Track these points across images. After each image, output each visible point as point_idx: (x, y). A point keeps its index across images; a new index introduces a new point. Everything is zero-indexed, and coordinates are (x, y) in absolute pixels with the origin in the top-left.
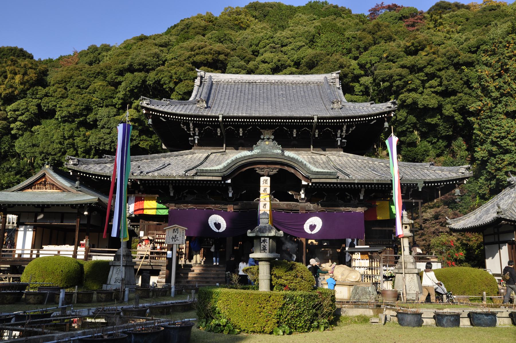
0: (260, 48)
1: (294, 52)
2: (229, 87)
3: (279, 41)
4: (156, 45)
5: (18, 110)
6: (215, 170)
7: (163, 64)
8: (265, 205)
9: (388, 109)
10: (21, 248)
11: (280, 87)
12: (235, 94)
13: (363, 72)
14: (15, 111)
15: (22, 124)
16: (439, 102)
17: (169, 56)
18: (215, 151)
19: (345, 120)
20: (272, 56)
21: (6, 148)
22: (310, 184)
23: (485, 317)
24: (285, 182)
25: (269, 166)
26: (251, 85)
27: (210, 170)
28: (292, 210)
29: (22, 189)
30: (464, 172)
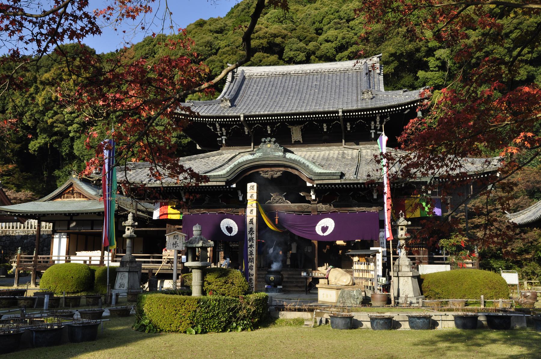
0: (324, 25)
1: (362, 26)
2: (261, 80)
3: (345, 15)
4: (211, 31)
5: (74, 113)
6: (219, 175)
7: (216, 54)
8: (252, 210)
10: (57, 255)
11: (315, 77)
12: (266, 89)
14: (71, 113)
15: (79, 126)
16: (528, 72)
17: (222, 44)
18: (243, 151)
19: (373, 112)
20: (336, 34)
21: (67, 151)
22: (315, 186)
23: (417, 321)
24: (290, 183)
25: (273, 169)
26: (285, 77)
28: (303, 212)
29: (53, 199)
30: (496, 164)
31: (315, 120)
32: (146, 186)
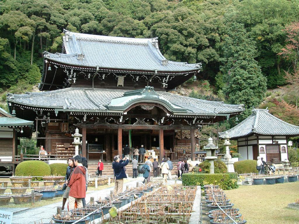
9: (197, 69)
10: (248, 144)
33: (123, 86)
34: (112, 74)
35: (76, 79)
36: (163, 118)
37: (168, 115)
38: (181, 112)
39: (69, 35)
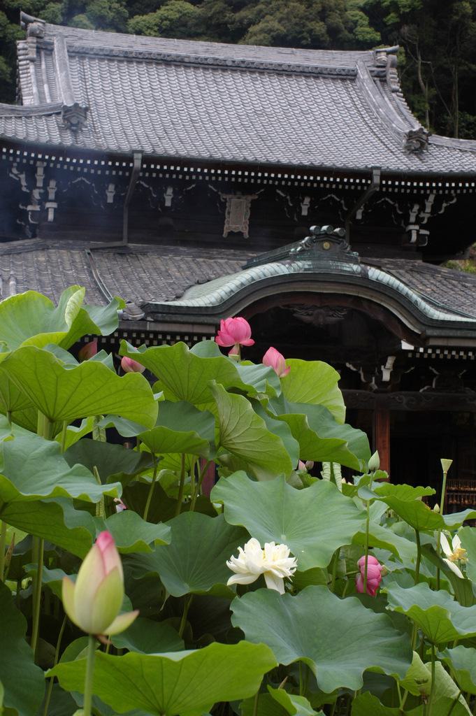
13: (378, 37)
27: (188, 307)
31: (280, 187)
32: (295, 315)
33: (246, 236)
34: (202, 186)
35: (55, 205)
36: (390, 361)
37: (406, 346)
38: (459, 333)
39: (41, 38)
